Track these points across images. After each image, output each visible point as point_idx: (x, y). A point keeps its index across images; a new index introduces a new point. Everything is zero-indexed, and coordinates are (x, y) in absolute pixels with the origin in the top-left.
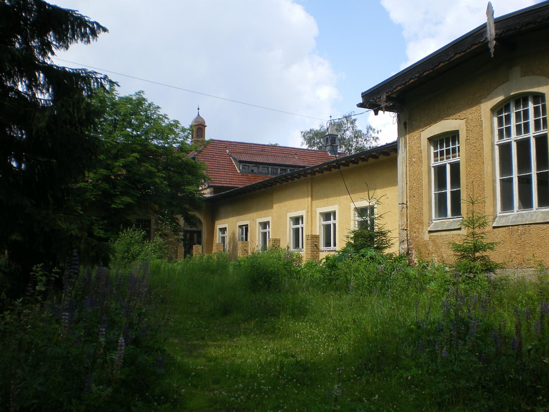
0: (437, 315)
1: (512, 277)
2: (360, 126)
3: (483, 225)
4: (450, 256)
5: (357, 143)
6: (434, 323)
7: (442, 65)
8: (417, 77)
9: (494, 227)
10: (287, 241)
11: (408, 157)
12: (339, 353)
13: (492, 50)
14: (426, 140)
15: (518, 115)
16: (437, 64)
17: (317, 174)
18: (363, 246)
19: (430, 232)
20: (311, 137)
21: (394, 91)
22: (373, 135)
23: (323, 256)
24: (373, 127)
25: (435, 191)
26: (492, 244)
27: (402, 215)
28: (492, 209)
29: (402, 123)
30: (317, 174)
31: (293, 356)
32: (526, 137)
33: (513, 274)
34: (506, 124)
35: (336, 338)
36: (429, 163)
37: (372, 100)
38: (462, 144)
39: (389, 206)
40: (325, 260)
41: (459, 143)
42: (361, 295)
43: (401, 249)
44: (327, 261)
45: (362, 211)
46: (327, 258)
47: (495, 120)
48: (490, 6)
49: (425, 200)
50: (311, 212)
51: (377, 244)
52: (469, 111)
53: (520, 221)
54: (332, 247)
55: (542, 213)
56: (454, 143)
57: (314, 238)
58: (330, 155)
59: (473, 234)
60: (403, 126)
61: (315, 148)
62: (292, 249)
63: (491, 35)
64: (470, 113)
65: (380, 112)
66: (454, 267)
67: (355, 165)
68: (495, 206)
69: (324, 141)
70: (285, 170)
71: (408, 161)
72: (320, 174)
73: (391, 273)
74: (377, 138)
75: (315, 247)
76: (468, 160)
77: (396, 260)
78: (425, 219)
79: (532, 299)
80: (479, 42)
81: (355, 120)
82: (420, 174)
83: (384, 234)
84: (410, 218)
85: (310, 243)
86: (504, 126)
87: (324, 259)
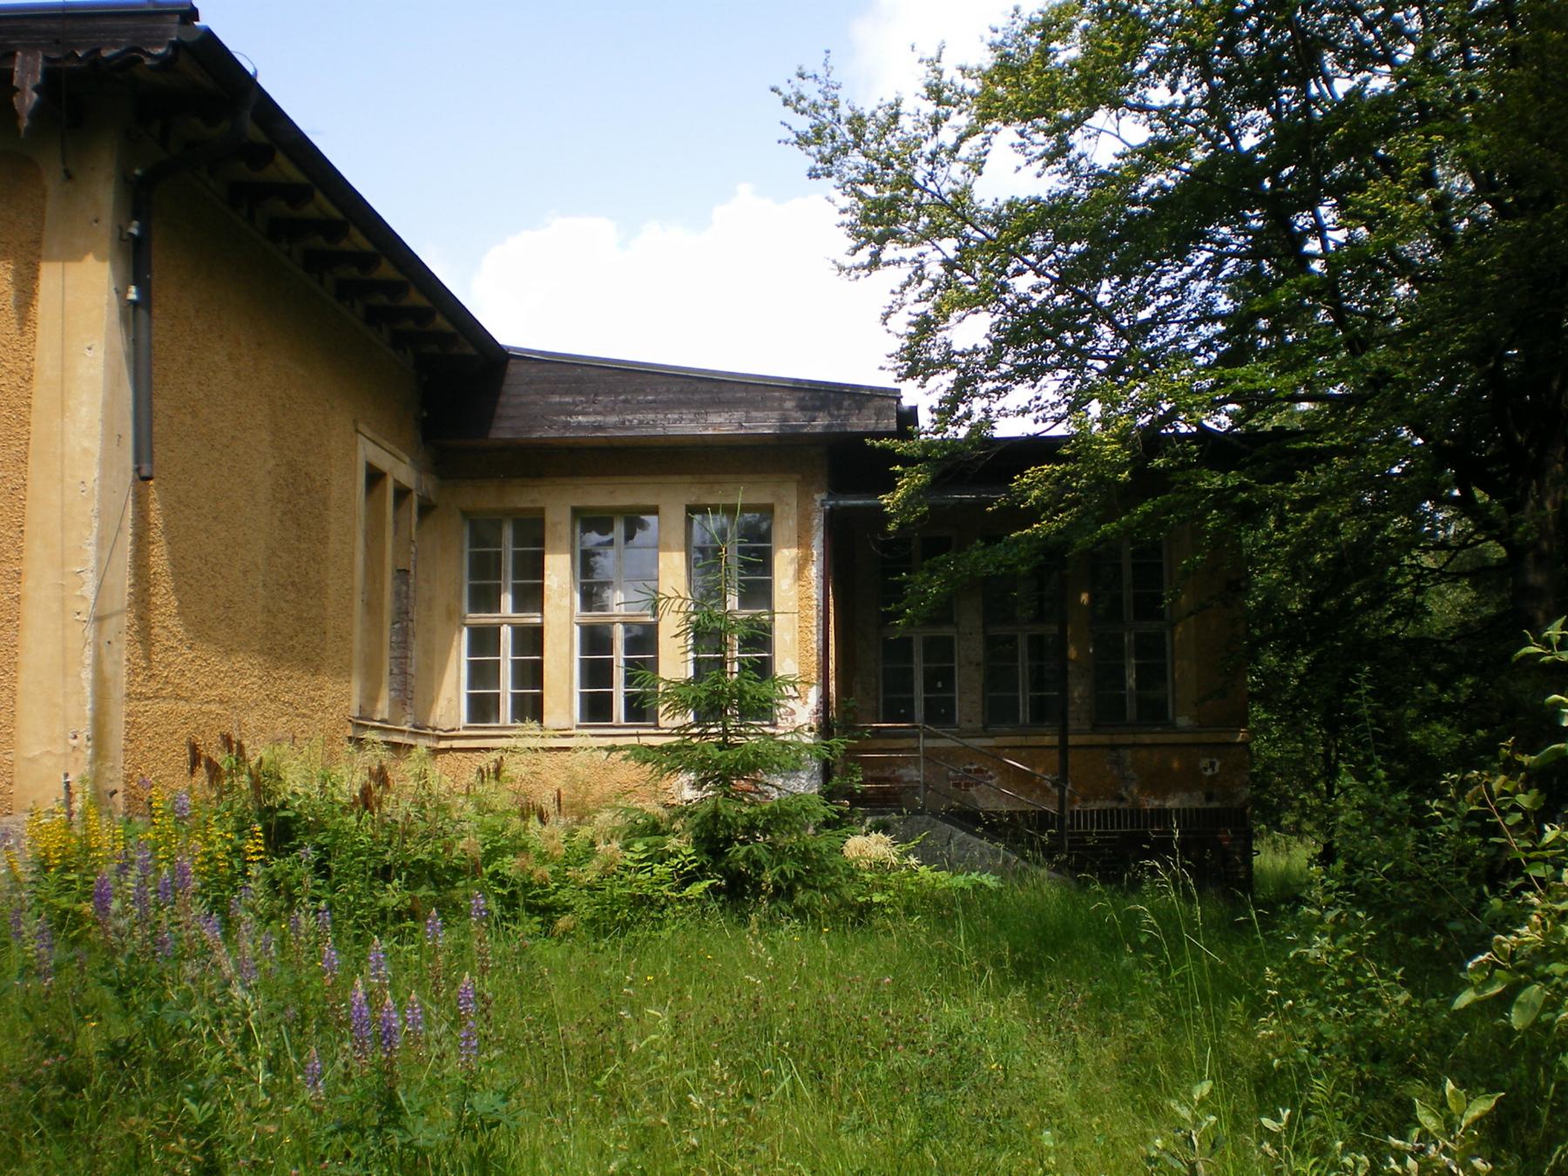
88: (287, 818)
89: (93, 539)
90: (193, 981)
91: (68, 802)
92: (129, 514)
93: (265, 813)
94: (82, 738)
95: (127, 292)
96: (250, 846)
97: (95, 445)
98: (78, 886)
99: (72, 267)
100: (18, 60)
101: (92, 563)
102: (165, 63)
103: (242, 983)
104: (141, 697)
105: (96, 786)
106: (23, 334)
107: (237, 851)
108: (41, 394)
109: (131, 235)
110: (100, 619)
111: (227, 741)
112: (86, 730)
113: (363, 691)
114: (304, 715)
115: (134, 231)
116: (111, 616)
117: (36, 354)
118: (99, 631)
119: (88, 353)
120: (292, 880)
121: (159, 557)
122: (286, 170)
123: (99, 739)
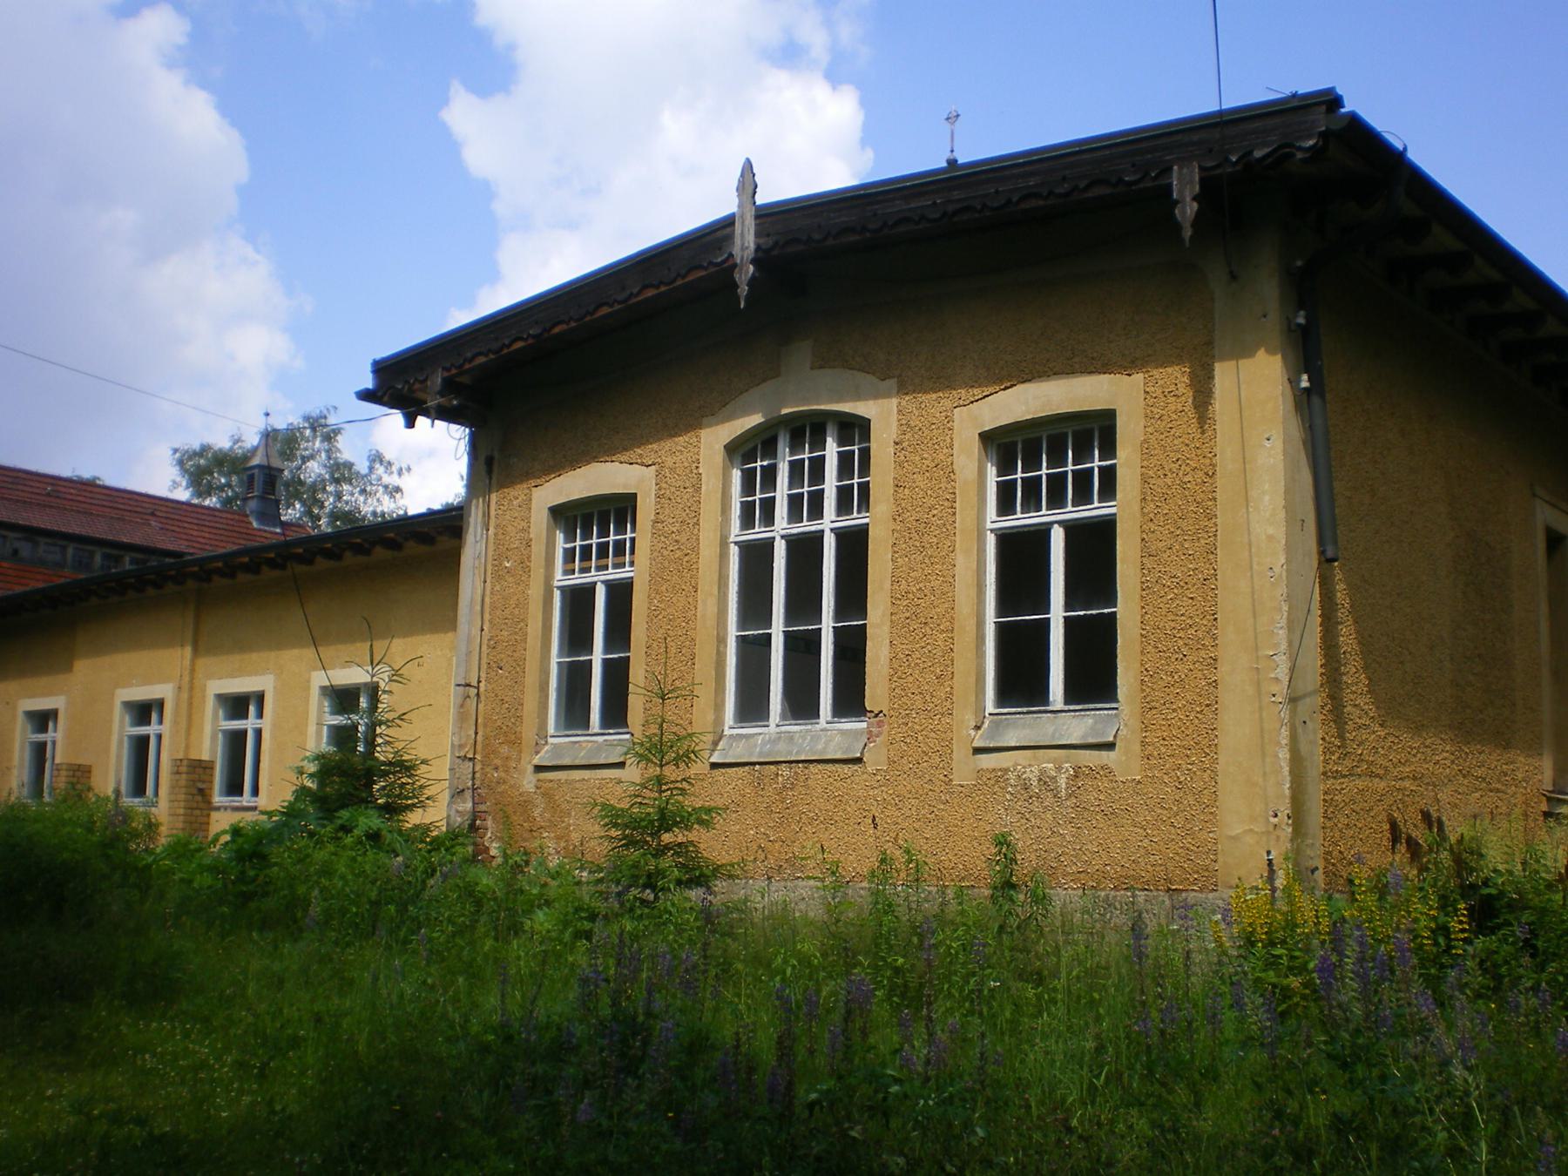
0: (558, 1005)
1: (758, 902)
2: (350, 449)
3: (686, 758)
4: (593, 838)
5: (339, 496)
6: (547, 1027)
7: (605, 310)
8: (533, 337)
9: (714, 766)
10: (110, 777)
11: (490, 553)
12: (274, 1112)
13: (743, 290)
14: (546, 512)
15: (796, 468)
16: (591, 308)
17: (216, 578)
18: (345, 801)
19: (539, 769)
20: (203, 467)
21: (467, 366)
22: (386, 479)
23: (221, 822)
24: (388, 456)
25: (560, 655)
26: (709, 811)
27: (462, 717)
28: (710, 717)
29: (482, 459)
30: (216, 578)
31: (140, 1122)
32: (813, 528)
33: (759, 894)
34: (762, 492)
35: (265, 1065)
36: (549, 577)
37: (404, 384)
38: (643, 533)
39: (430, 692)
40: (228, 838)
41: (634, 530)
42: (336, 943)
43: (453, 813)
44: (233, 841)
45: (344, 699)
46: (236, 831)
47: (736, 475)
48: (748, 168)
49: (531, 679)
50: (190, 691)
51: (388, 796)
52: (668, 444)
53: (783, 752)
54: (246, 799)
55: (843, 732)
56: (621, 529)
57: (201, 768)
58: (255, 525)
59: (659, 780)
60: (483, 468)
61: (211, 501)
62: (128, 801)
63: (743, 248)
64: (673, 450)
65: (422, 421)
66: (600, 870)
67: (332, 564)
68: (719, 707)
69: (241, 481)
70: (118, 560)
71: (489, 568)
72: (225, 581)
73: (424, 882)
74: (398, 489)
75: (198, 797)
76: (656, 578)
77: (437, 844)
78: (528, 732)
79: (810, 964)
80: (710, 263)
81: (337, 432)
82: (522, 604)
83: (408, 769)
84: (485, 726)
85: (183, 783)
86: (758, 496)
87: (224, 832)
88: (1490, 895)
89: (1284, 622)
90: (1416, 1058)
91: (1271, 877)
92: (1317, 596)
93: (1468, 890)
94: (1282, 816)
95: (1299, 381)
96: (1454, 925)
97: (1279, 532)
98: (1284, 961)
99: (1243, 363)
100: (1175, 175)
101: (1284, 646)
102: (1316, 154)
103: (1463, 1062)
104: (1337, 775)
105: (1296, 864)
106: (1203, 433)
107: (1444, 930)
108: (1224, 485)
109: (1299, 325)
110: (1293, 700)
111: (1426, 816)
112: (1285, 809)
113: (1555, 763)
114: (1498, 791)
115: (1301, 320)
116: (1305, 696)
117: (1217, 450)
118: (1293, 713)
119: (1267, 444)
120: (1499, 958)
121: (1347, 637)
122: (1442, 239)
123: (1298, 816)
